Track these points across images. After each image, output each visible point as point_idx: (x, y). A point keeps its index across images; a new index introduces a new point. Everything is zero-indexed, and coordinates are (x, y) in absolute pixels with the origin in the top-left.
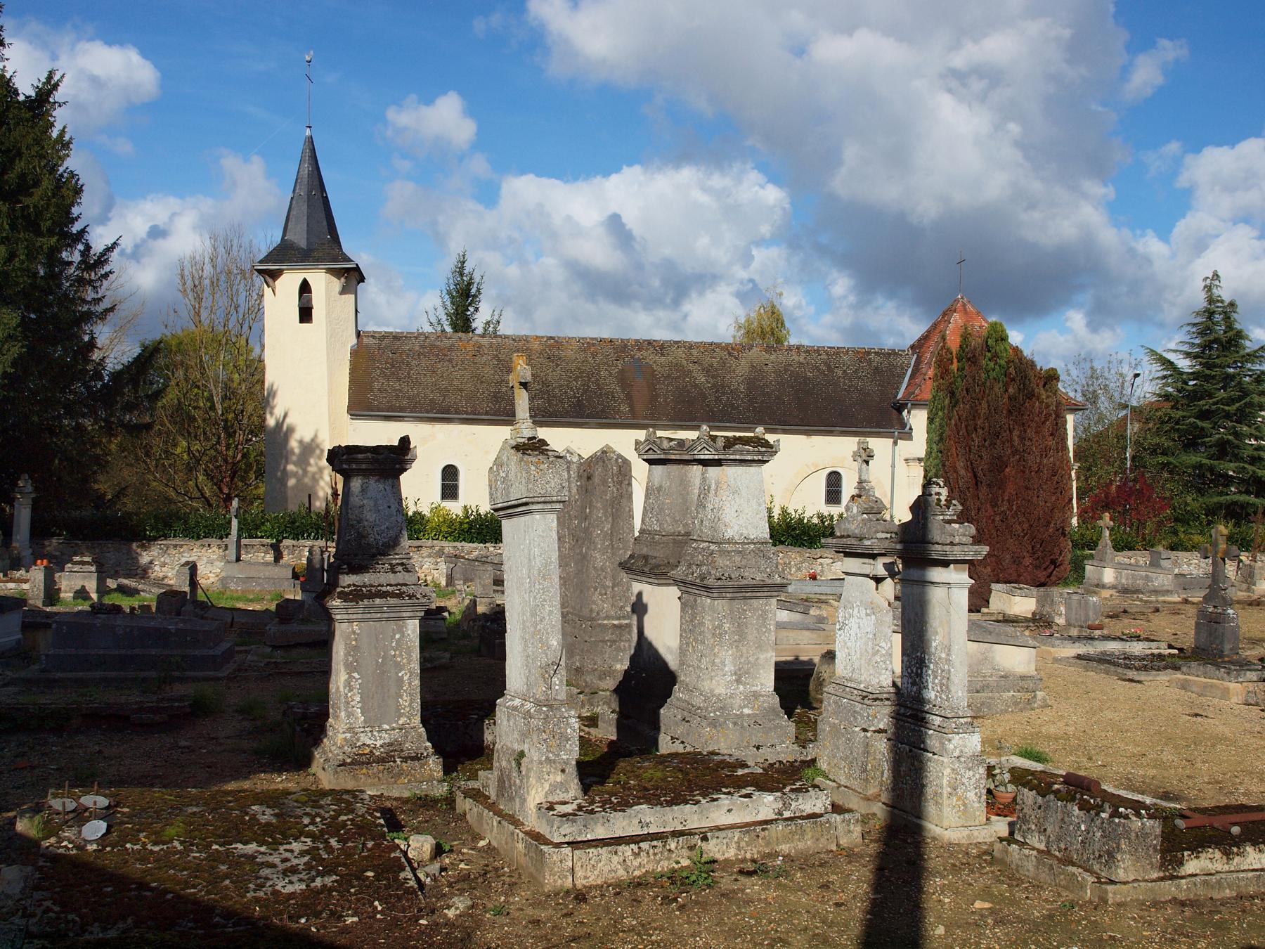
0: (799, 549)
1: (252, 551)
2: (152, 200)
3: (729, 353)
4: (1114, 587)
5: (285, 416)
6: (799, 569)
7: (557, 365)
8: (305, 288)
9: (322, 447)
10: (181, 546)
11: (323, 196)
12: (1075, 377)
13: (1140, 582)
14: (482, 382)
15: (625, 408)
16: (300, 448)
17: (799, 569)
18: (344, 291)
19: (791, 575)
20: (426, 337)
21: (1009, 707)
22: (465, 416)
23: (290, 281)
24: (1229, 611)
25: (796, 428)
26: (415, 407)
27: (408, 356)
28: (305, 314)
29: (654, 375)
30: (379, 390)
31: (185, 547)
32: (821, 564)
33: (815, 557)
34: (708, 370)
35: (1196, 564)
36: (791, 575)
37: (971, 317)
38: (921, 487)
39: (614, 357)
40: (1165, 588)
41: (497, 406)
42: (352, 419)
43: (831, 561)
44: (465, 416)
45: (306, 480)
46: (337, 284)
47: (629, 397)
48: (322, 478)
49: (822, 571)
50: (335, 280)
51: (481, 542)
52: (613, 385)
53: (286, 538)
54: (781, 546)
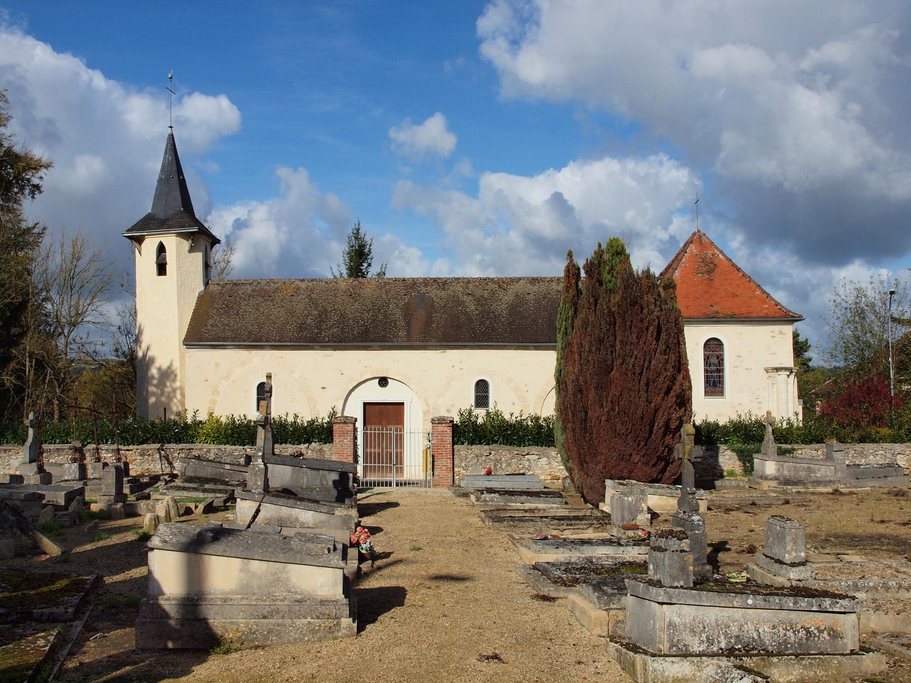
0: (508, 447)
1: (63, 453)
2: (239, 205)
3: (499, 286)
4: (775, 478)
5: (148, 349)
6: (509, 465)
7: (356, 301)
8: (161, 249)
9: (175, 373)
10: (10, 451)
11: (179, 179)
12: (843, 297)
13: (803, 474)
15: (402, 333)
16: (158, 373)
17: (509, 465)
18: (192, 250)
19: (503, 469)
20: (259, 283)
21: (304, 635)
22: (273, 343)
23: (150, 244)
24: (693, 518)
25: (543, 344)
26: (236, 337)
27: (240, 298)
28: (162, 269)
29: (432, 306)
30: (212, 325)
31: (12, 451)
32: (528, 460)
33: (523, 454)
34: (479, 301)
35: (882, 454)
36: (503, 469)
37: (704, 247)
39: (403, 292)
40: (827, 479)
41: (300, 335)
42: (188, 348)
43: (537, 457)
44: (273, 343)
45: (163, 399)
46: (186, 244)
47: (408, 324)
48: (175, 396)
49: (529, 466)
50: (185, 241)
51: (240, 445)
52: (398, 314)
53: (90, 443)
54: (494, 445)
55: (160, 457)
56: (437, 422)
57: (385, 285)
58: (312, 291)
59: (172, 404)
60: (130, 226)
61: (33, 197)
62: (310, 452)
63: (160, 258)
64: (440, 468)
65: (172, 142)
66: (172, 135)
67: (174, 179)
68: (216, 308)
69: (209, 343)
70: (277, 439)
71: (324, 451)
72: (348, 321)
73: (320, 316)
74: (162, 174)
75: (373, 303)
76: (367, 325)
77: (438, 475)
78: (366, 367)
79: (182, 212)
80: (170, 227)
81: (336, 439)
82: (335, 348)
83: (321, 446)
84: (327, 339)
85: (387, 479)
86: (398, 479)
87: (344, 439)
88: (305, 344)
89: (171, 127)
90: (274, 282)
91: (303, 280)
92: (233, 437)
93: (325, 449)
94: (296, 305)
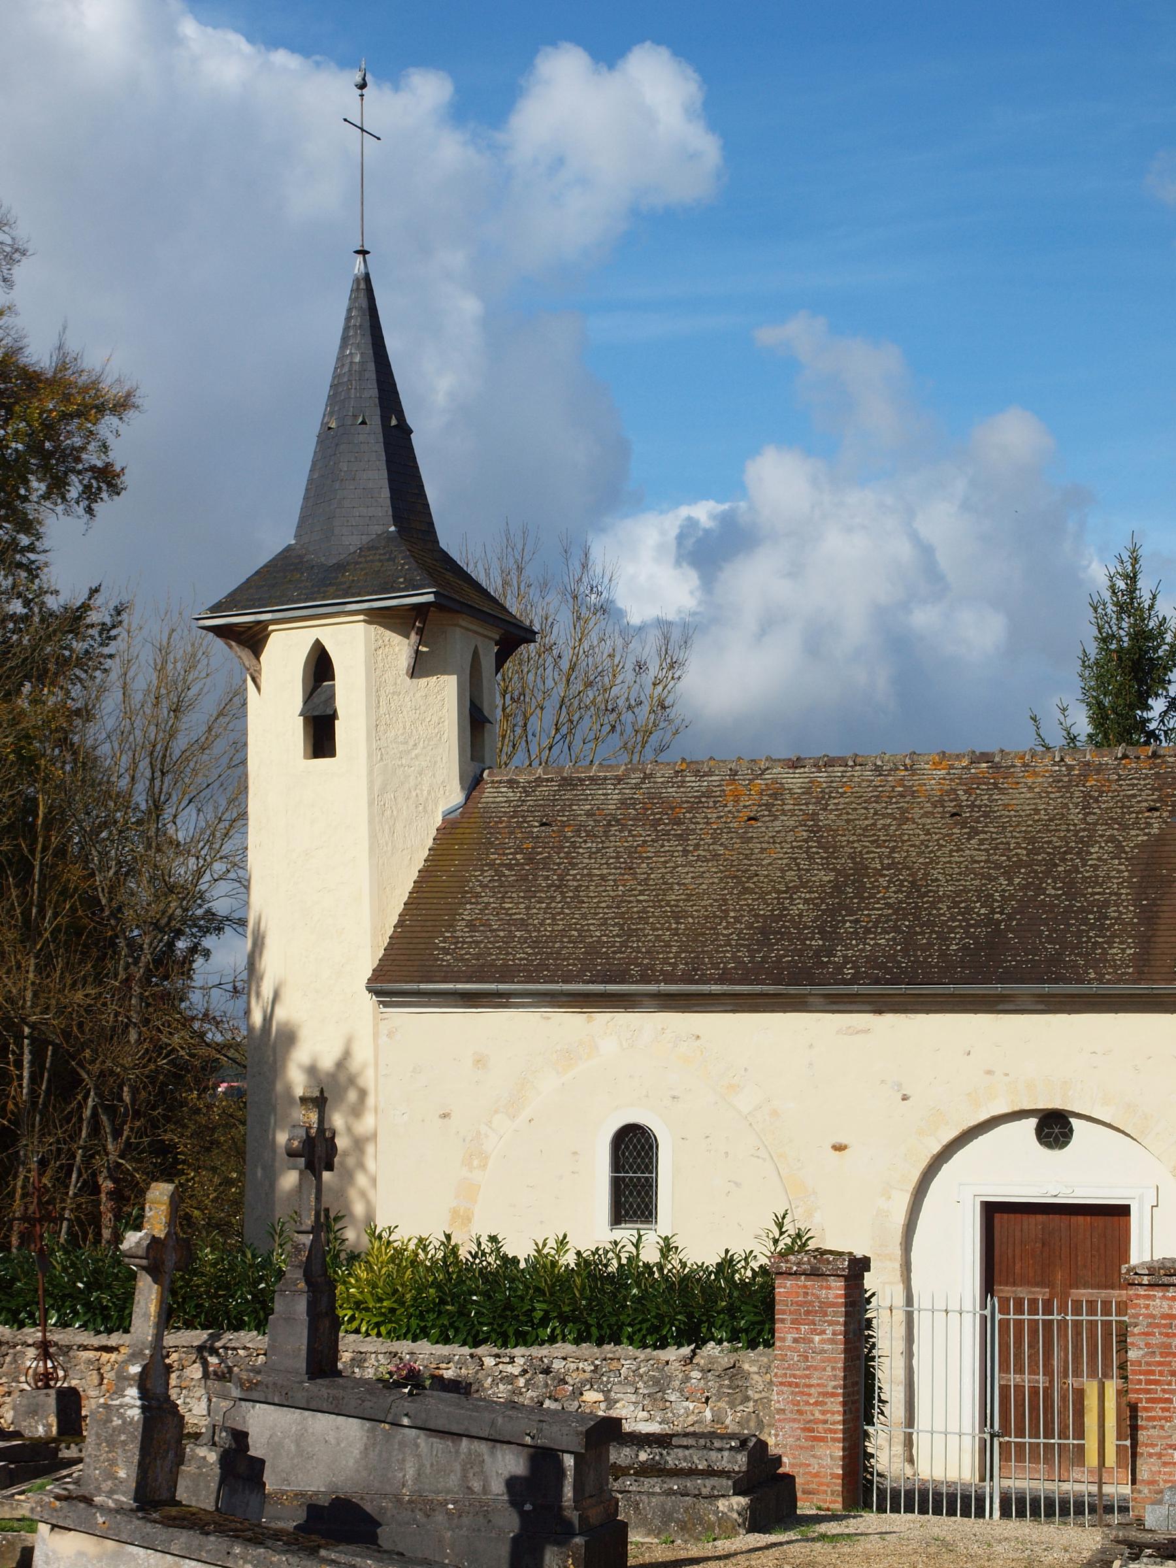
9: (361, 1082)
14: (746, 890)
15: (1122, 951)
18: (419, 668)
22: (663, 987)
26: (543, 966)
30: (471, 926)
38: (1074, 1128)
39: (1148, 797)
44: (663, 987)
51: (464, 1344)
55: (206, 1375)
56: (1145, 1280)
57: (1084, 776)
58: (823, 801)
59: (353, 1194)
60: (220, 593)
61: (89, 510)
62: (696, 1374)
63: (318, 699)
64: (1160, 1456)
65: (365, 304)
66: (367, 278)
67: (366, 428)
68: (491, 865)
69: (450, 986)
70: (588, 1326)
71: (746, 1376)
72: (933, 905)
73: (837, 888)
74: (331, 414)
75: (1032, 841)
76: (999, 922)
77: (1152, 1482)
78: (989, 1072)
79: (389, 538)
80: (349, 591)
81: (785, 1332)
82: (880, 1005)
83: (734, 1357)
84: (849, 972)
85: (1066, 1487)
86: (1006, 1483)
87: (814, 1332)
88: (771, 989)
89: (363, 253)
90: (696, 773)
91: (796, 764)
92: (440, 1313)
93: (746, 1367)
94: (763, 850)
